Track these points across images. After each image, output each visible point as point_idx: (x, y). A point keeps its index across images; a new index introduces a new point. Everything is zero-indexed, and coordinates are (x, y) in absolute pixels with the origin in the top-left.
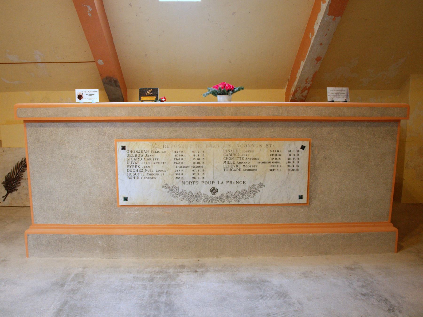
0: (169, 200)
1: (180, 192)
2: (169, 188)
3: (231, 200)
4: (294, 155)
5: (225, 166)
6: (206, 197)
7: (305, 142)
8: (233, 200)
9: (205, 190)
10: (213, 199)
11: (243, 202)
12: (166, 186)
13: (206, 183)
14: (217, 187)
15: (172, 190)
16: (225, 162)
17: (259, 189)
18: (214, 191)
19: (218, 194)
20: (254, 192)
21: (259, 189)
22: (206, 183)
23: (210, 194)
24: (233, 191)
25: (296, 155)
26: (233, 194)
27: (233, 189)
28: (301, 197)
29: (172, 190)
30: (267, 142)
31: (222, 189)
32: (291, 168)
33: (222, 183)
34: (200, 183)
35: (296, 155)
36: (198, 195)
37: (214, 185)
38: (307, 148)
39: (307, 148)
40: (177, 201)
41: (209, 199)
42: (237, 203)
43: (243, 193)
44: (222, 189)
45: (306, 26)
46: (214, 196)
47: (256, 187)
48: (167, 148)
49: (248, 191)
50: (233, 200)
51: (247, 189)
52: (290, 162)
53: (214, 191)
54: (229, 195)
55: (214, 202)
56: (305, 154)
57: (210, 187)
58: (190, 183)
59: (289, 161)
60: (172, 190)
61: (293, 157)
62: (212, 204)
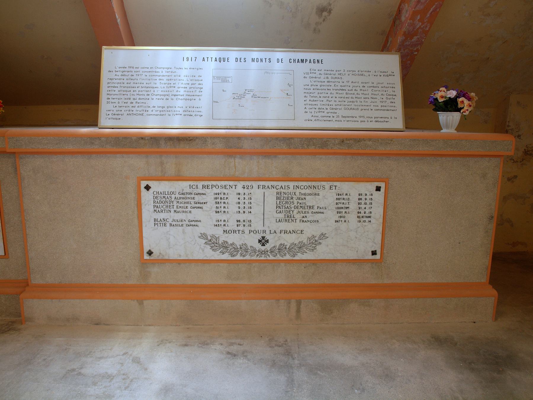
0: (210, 254)
1: (220, 243)
2: (207, 239)
3: (285, 255)
4: (365, 204)
5: (278, 203)
6: (254, 251)
7: (381, 183)
8: (287, 255)
9: (253, 241)
11: (299, 256)
12: (203, 236)
14: (268, 237)
15: (212, 242)
17: (320, 241)
18: (263, 241)
19: (268, 246)
21: (320, 241)
22: (255, 232)
23: (258, 246)
25: (368, 203)
26: (287, 247)
27: (289, 240)
29: (212, 242)
31: (273, 242)
33: (275, 232)
34: (247, 232)
35: (368, 203)
36: (244, 249)
37: (264, 235)
38: (383, 190)
40: (217, 255)
41: (257, 253)
43: (301, 247)
44: (273, 242)
45: (351, 258)
46: (263, 248)
48: (207, 190)
49: (306, 243)
50: (287, 255)
51: (305, 241)
52: (361, 199)
53: (263, 241)
54: (282, 248)
55: (263, 256)
57: (259, 237)
58: (235, 232)
59: (360, 197)
60: (210, 240)
61: (363, 199)
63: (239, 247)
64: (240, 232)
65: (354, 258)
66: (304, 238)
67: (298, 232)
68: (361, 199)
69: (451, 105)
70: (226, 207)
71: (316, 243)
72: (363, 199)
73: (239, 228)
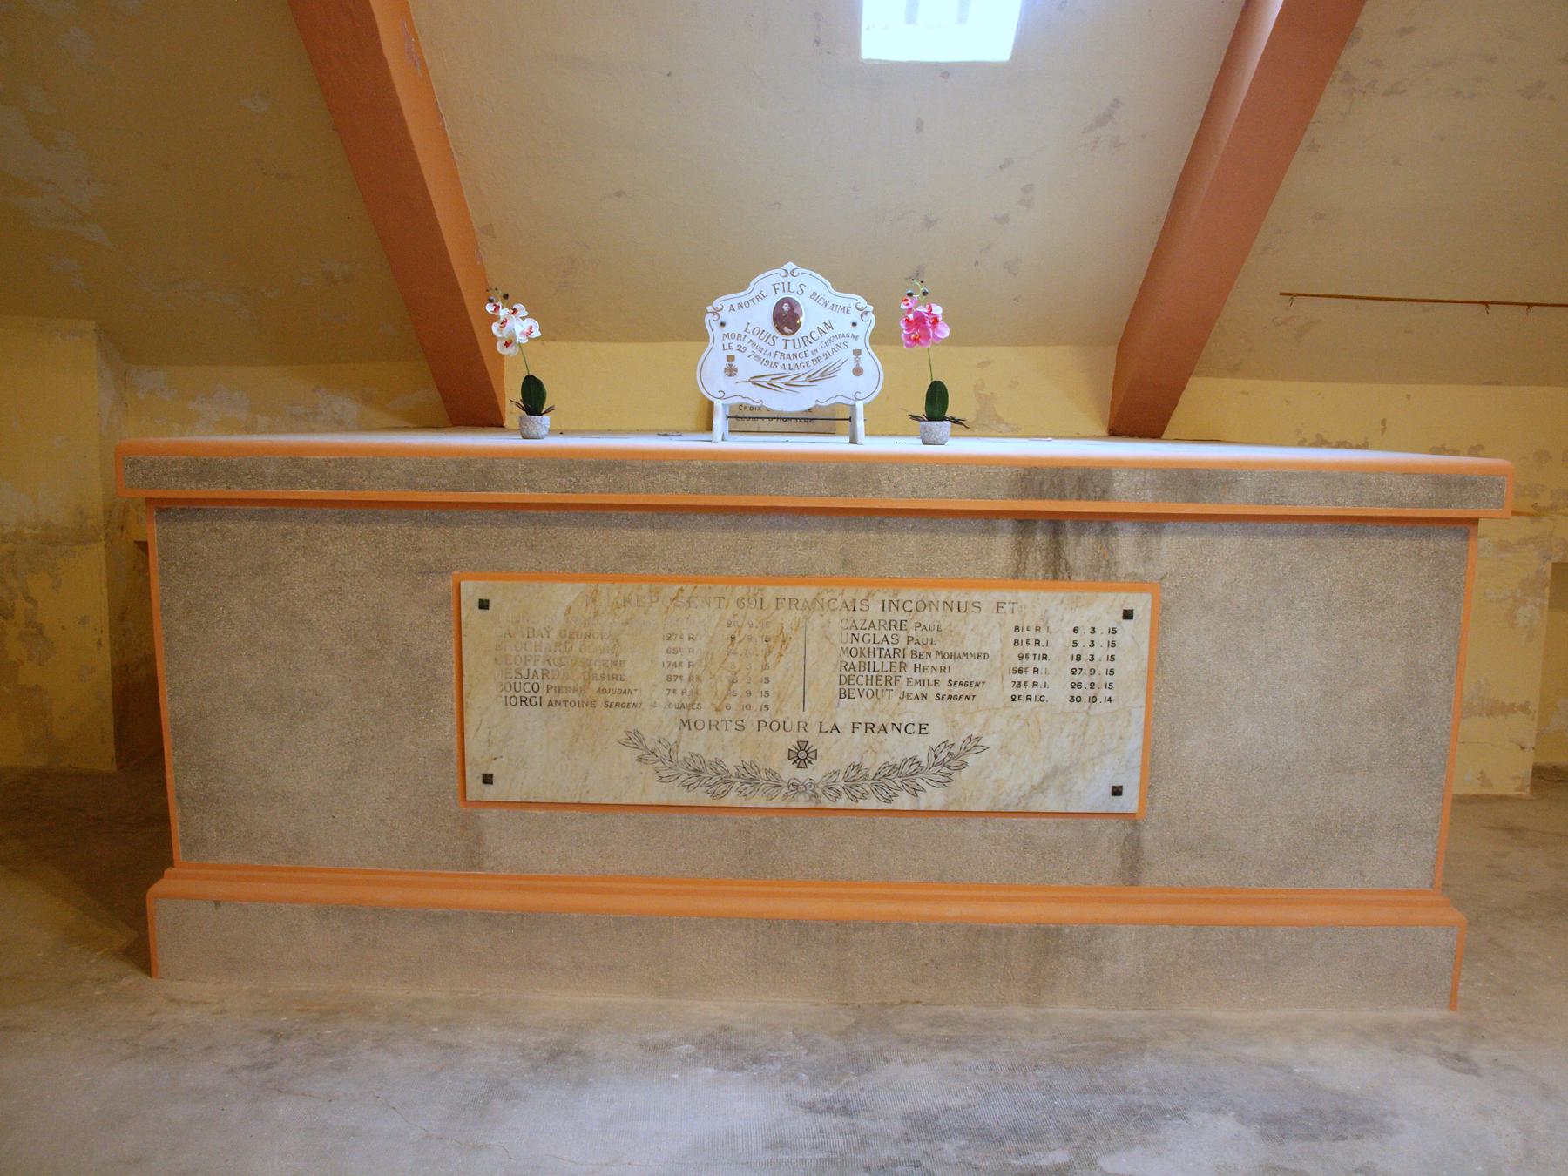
10: (795, 787)
13: (775, 726)
16: (843, 666)
18: (802, 756)
19: (814, 772)
20: (945, 770)
23: (789, 772)
24: (872, 764)
26: (872, 774)
28: (1117, 791)
30: (996, 595)
32: (1085, 693)
36: (750, 776)
37: (802, 736)
39: (1119, 805)
42: (888, 806)
47: (955, 750)
51: (923, 758)
52: (1079, 685)
54: (854, 778)
56: (1135, 636)
57: (788, 741)
59: (1077, 692)
61: (1085, 684)
62: (793, 805)
63: (733, 771)
64: (732, 726)
65: (1114, 356)
66: (919, 747)
67: (910, 729)
68: (1079, 685)
69: (497, 308)
70: (1041, 684)
71: (953, 763)
72: (1085, 684)
73: (727, 715)
